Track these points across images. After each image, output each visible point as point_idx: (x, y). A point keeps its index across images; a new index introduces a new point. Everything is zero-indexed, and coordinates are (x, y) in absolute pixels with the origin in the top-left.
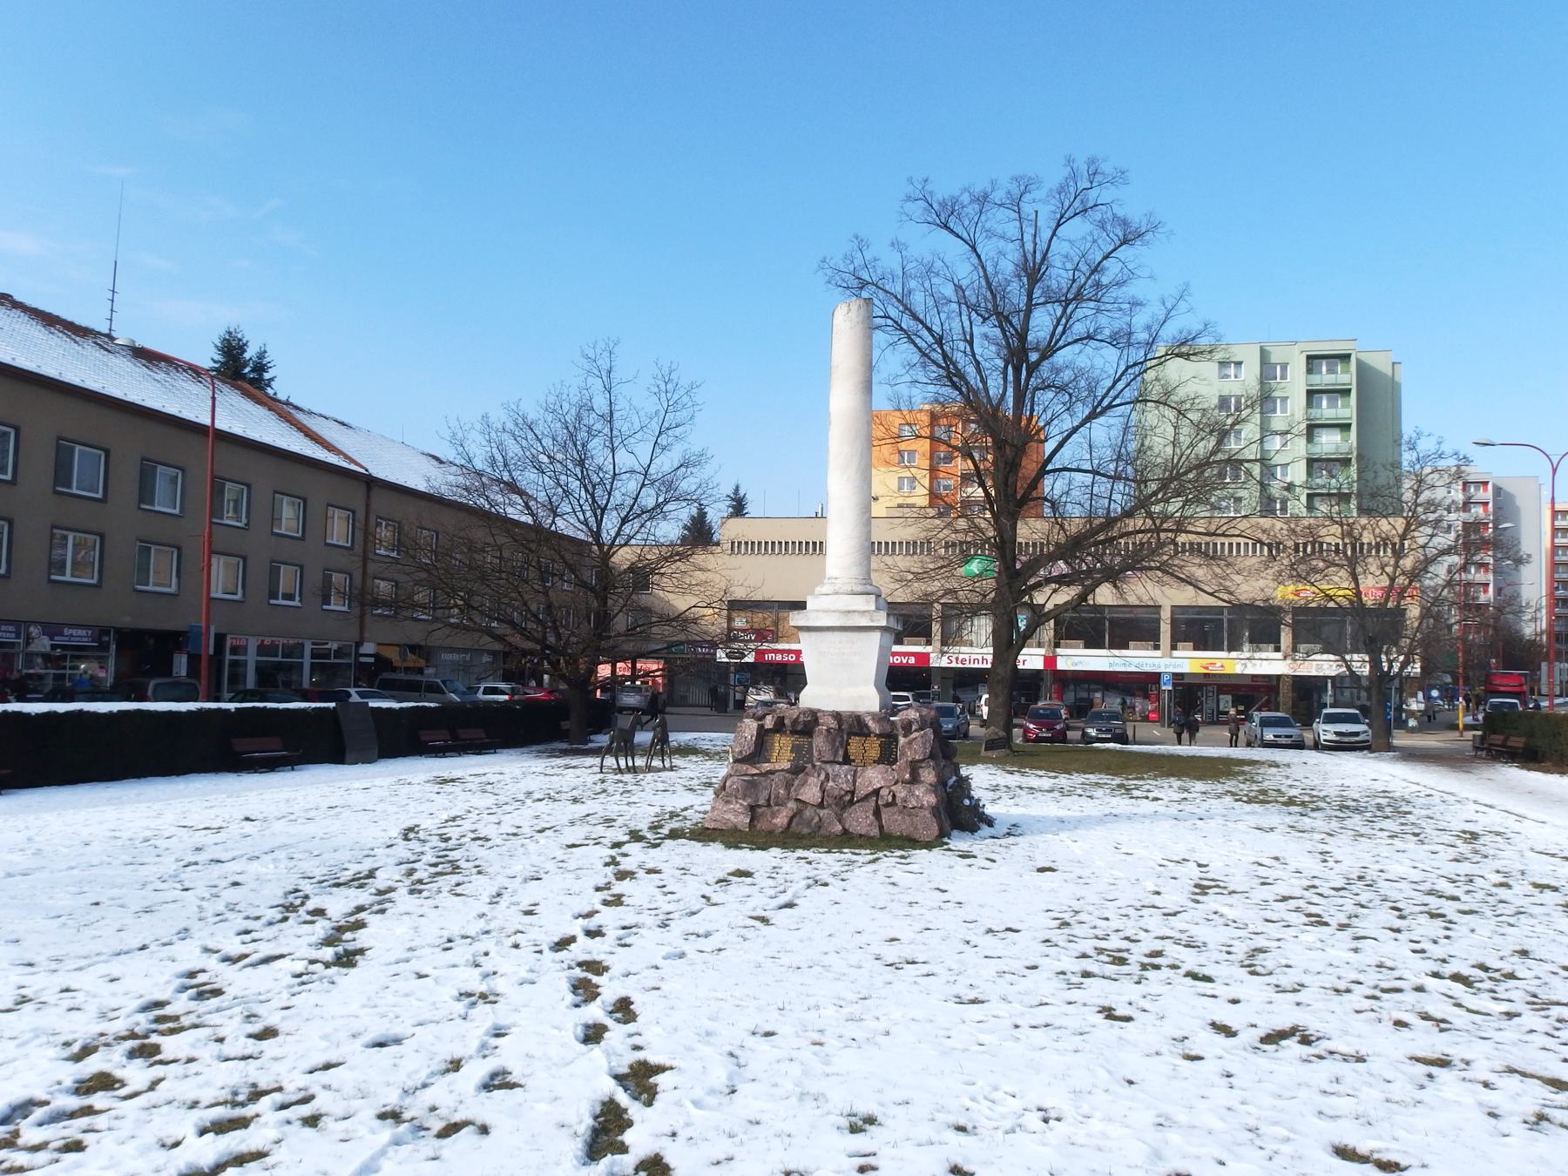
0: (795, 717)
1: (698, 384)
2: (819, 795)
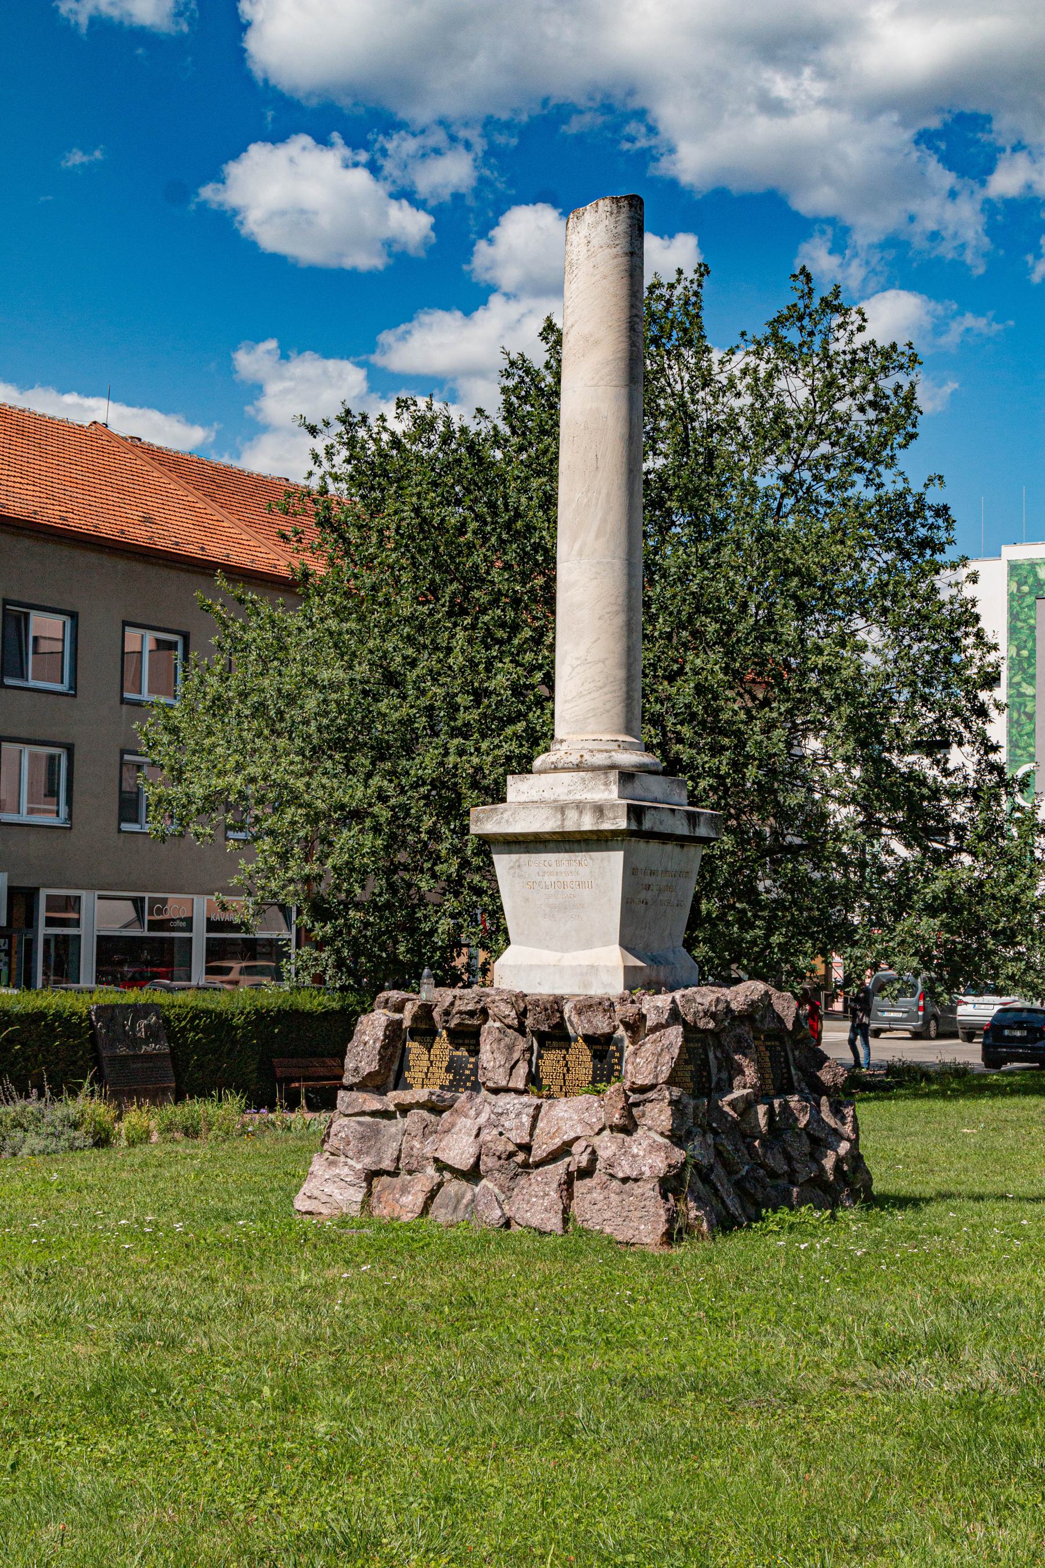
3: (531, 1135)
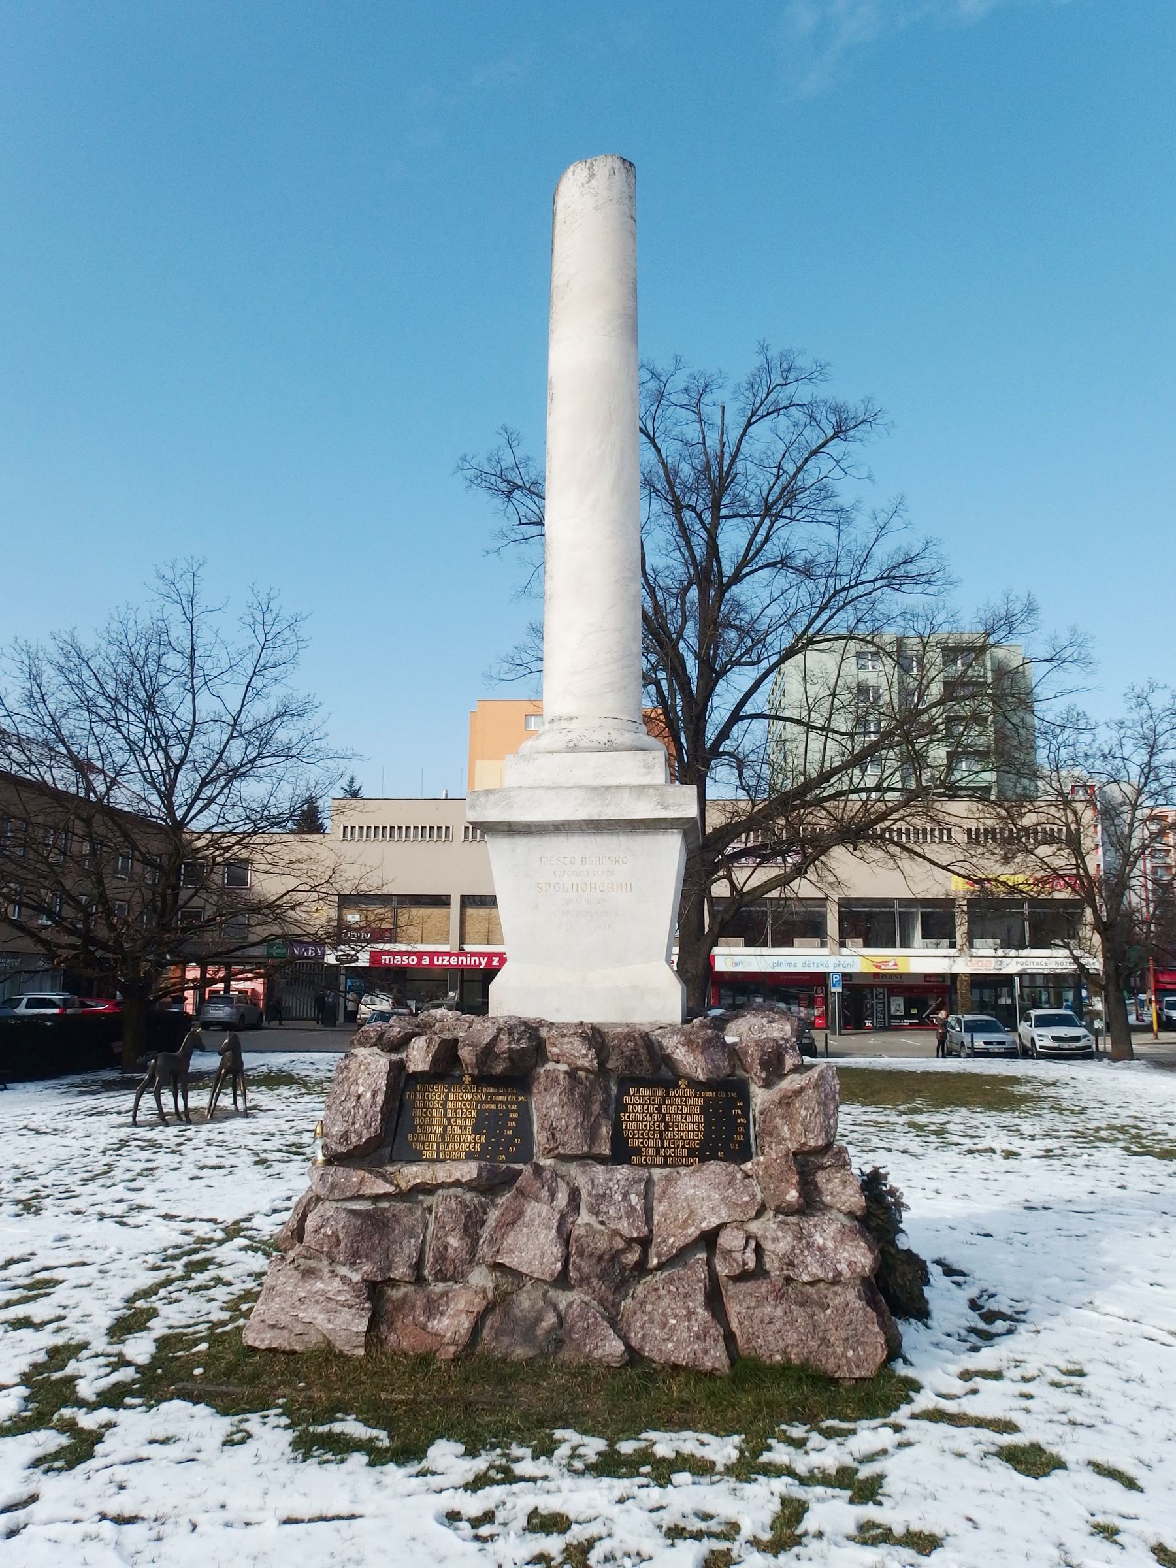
0: (486, 1039)
1: (304, 615)
2: (557, 1250)
3: (649, 1220)
